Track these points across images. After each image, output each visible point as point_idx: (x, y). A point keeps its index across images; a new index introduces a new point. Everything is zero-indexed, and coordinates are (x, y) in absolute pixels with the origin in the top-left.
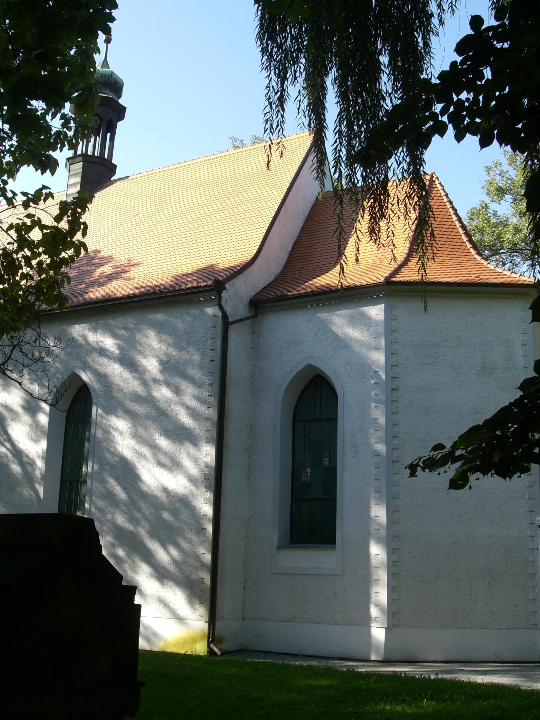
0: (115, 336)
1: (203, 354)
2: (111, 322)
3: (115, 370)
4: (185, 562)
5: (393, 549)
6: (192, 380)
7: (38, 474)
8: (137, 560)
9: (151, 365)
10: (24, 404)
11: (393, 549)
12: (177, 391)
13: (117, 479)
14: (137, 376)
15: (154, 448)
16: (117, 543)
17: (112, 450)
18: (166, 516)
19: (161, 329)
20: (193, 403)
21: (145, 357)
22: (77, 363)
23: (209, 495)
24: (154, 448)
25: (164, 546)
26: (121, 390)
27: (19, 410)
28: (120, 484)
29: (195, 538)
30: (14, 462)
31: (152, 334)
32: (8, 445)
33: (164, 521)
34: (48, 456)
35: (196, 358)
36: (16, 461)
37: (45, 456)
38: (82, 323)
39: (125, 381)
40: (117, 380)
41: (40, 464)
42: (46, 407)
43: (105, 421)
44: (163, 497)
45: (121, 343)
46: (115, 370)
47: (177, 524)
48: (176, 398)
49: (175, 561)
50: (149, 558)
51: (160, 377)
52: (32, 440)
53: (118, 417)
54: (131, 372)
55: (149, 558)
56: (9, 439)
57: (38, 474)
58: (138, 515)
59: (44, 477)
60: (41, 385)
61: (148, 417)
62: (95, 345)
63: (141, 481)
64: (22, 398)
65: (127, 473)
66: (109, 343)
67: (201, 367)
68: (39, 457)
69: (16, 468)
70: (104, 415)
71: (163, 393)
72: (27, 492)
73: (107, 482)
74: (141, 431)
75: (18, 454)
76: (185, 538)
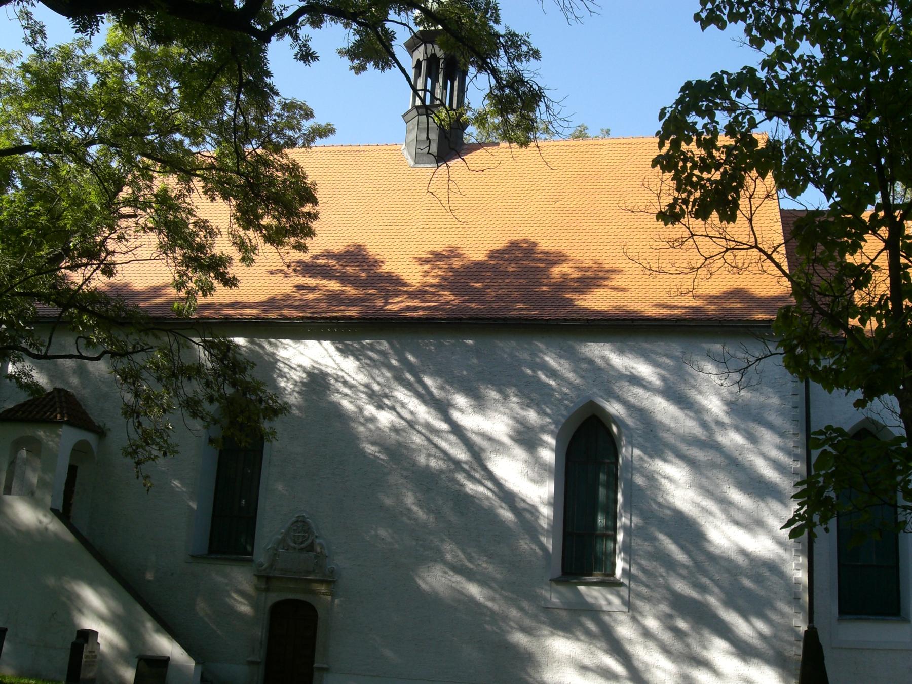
0: (655, 364)
1: (782, 397)
2: (646, 345)
3: (663, 409)
4: (775, 636)
5: (403, 116)
6: (770, 426)
7: (544, 523)
8: (706, 633)
9: (714, 405)
10: (512, 433)
11: (403, 116)
12: (752, 438)
13: (670, 535)
14: (692, 414)
15: (725, 503)
16: (673, 612)
17: (661, 500)
18: (747, 583)
19: (721, 361)
20: (774, 453)
21: (700, 392)
22: (595, 390)
23: (803, 560)
24: (725, 503)
25: (745, 615)
26: (668, 429)
27: (506, 440)
28: (676, 541)
29: (787, 609)
30: (501, 507)
31: (709, 367)
32: (490, 484)
33: (743, 588)
34: (553, 503)
35: (775, 401)
36: (503, 505)
37: (552, 501)
38: (600, 342)
39: (676, 419)
40: (659, 417)
41: (546, 511)
42: (550, 440)
43: (646, 465)
44: (740, 560)
45: (663, 372)
46: (663, 409)
47: (762, 593)
48: (751, 446)
49: (762, 637)
50: (725, 632)
51: (726, 420)
52: (533, 481)
53: (665, 460)
54: (681, 409)
55: (725, 632)
56: (491, 476)
57: (544, 523)
58: (705, 580)
59: (553, 526)
60: (541, 413)
61: (713, 465)
62: (624, 371)
63: (709, 541)
64: (508, 425)
65: (687, 531)
66: (644, 370)
67: (781, 413)
68: (543, 503)
69: (507, 515)
70: (646, 458)
71: (733, 439)
72: (525, 545)
73: (656, 539)
74: (705, 482)
75: (508, 497)
76: (775, 609)
